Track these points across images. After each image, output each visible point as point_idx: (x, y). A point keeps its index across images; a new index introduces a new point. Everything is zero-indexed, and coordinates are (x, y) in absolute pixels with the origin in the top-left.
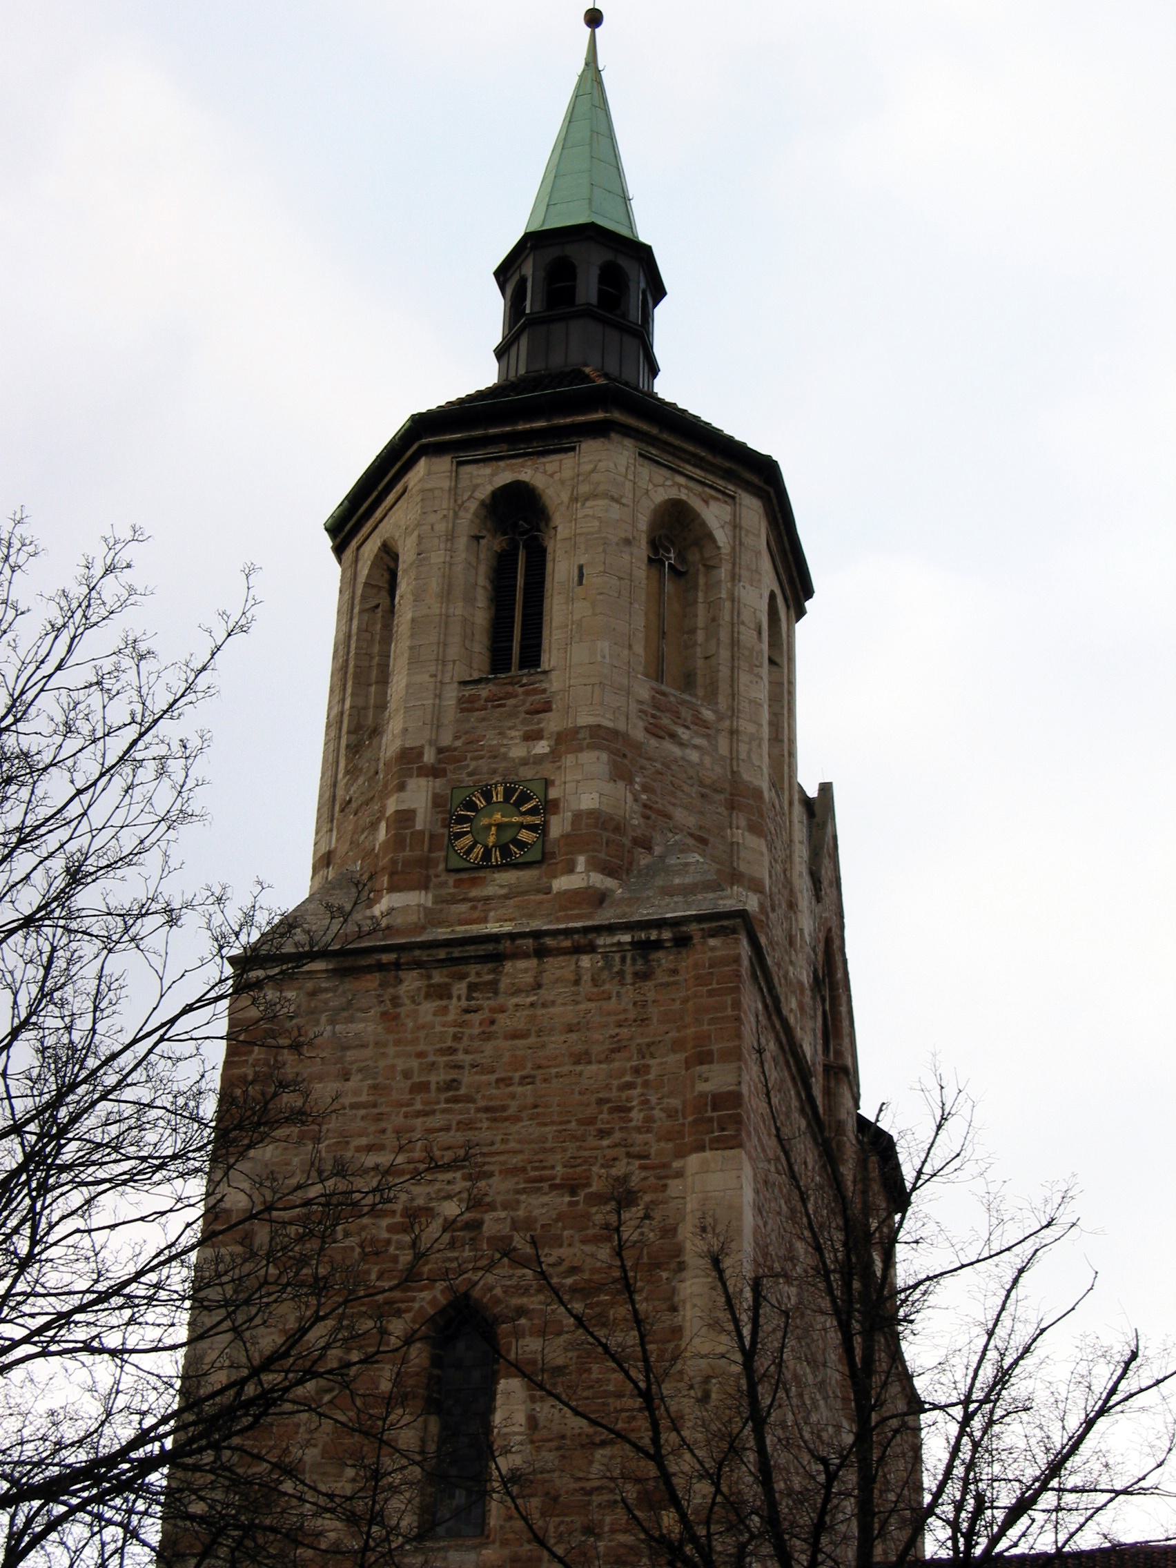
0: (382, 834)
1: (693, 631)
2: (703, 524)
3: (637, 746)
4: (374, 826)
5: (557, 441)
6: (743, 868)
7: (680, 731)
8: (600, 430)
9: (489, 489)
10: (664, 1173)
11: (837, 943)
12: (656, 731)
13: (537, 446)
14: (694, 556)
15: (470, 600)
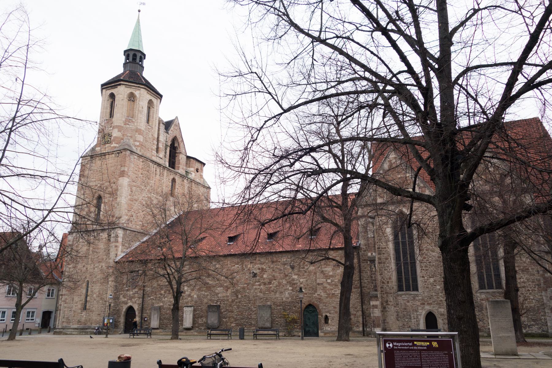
3: (122, 127)
8: (120, 85)
10: (118, 180)
12: (125, 124)
15: (107, 109)
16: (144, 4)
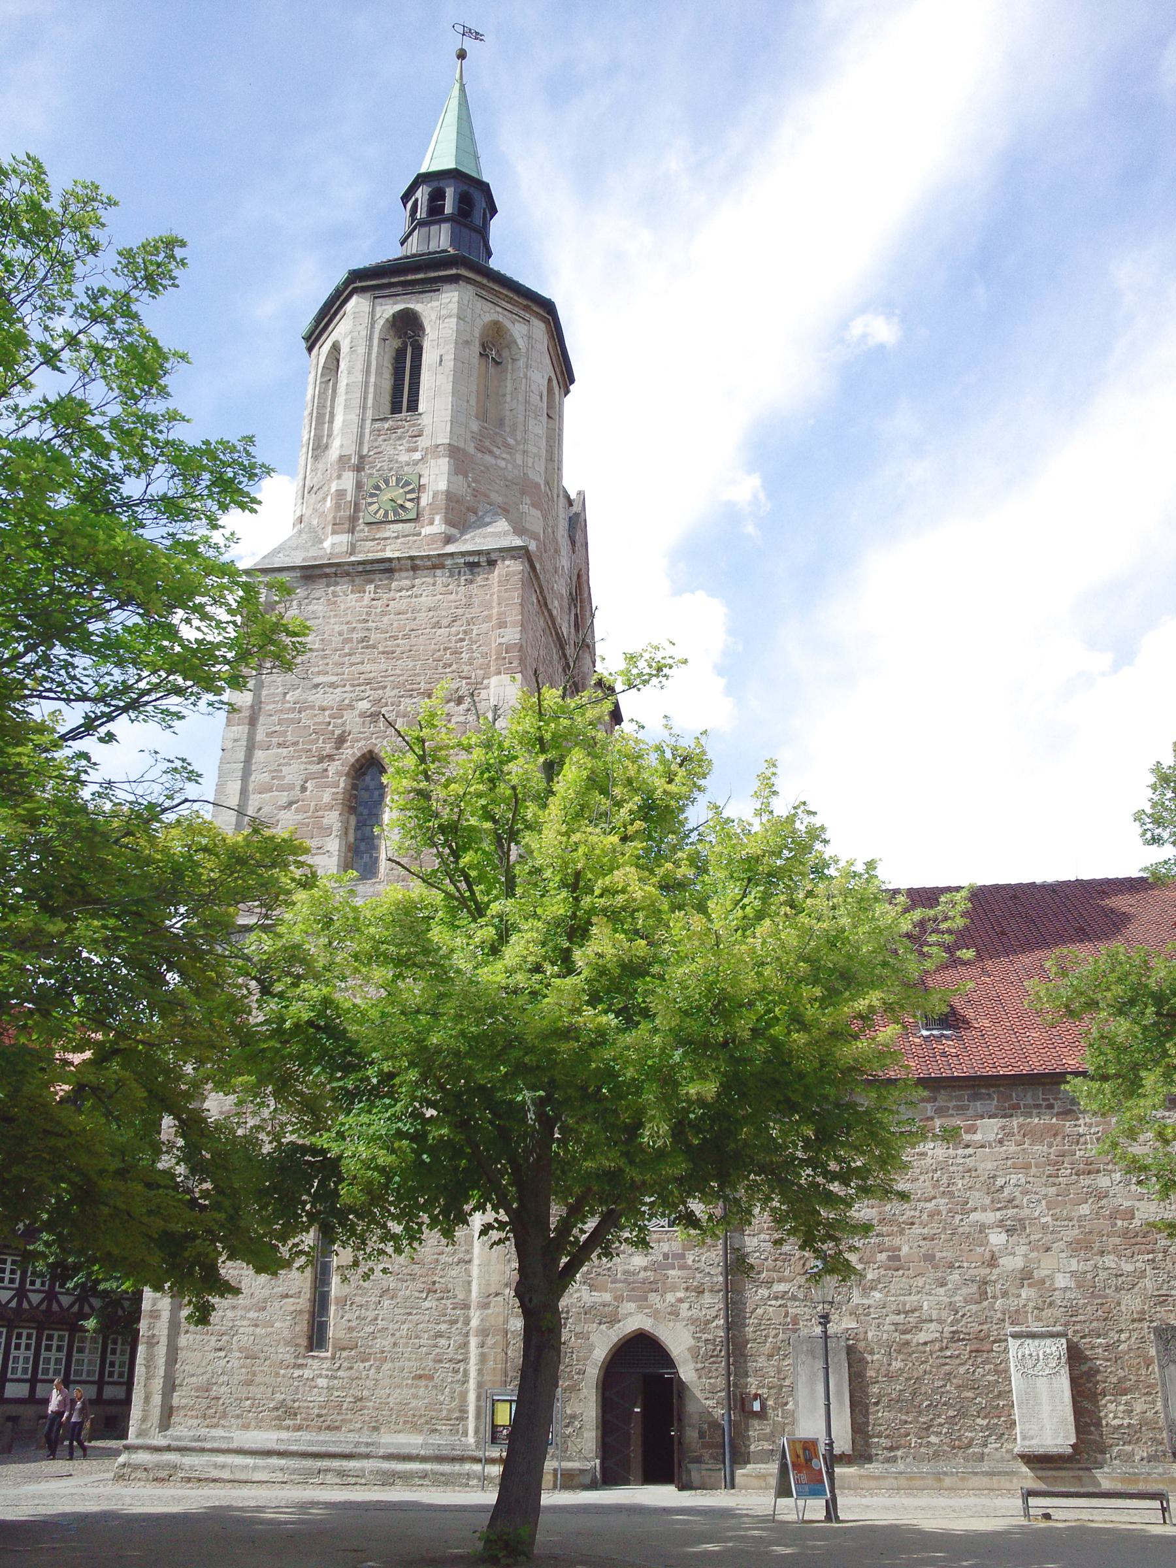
0: (329, 503)
1: (504, 395)
2: (511, 335)
4: (324, 499)
5: (431, 286)
6: (528, 526)
7: (495, 449)
8: (454, 279)
9: (391, 312)
11: (584, 578)
12: (481, 449)
13: (418, 288)
14: (505, 353)
16: (478, 36)
